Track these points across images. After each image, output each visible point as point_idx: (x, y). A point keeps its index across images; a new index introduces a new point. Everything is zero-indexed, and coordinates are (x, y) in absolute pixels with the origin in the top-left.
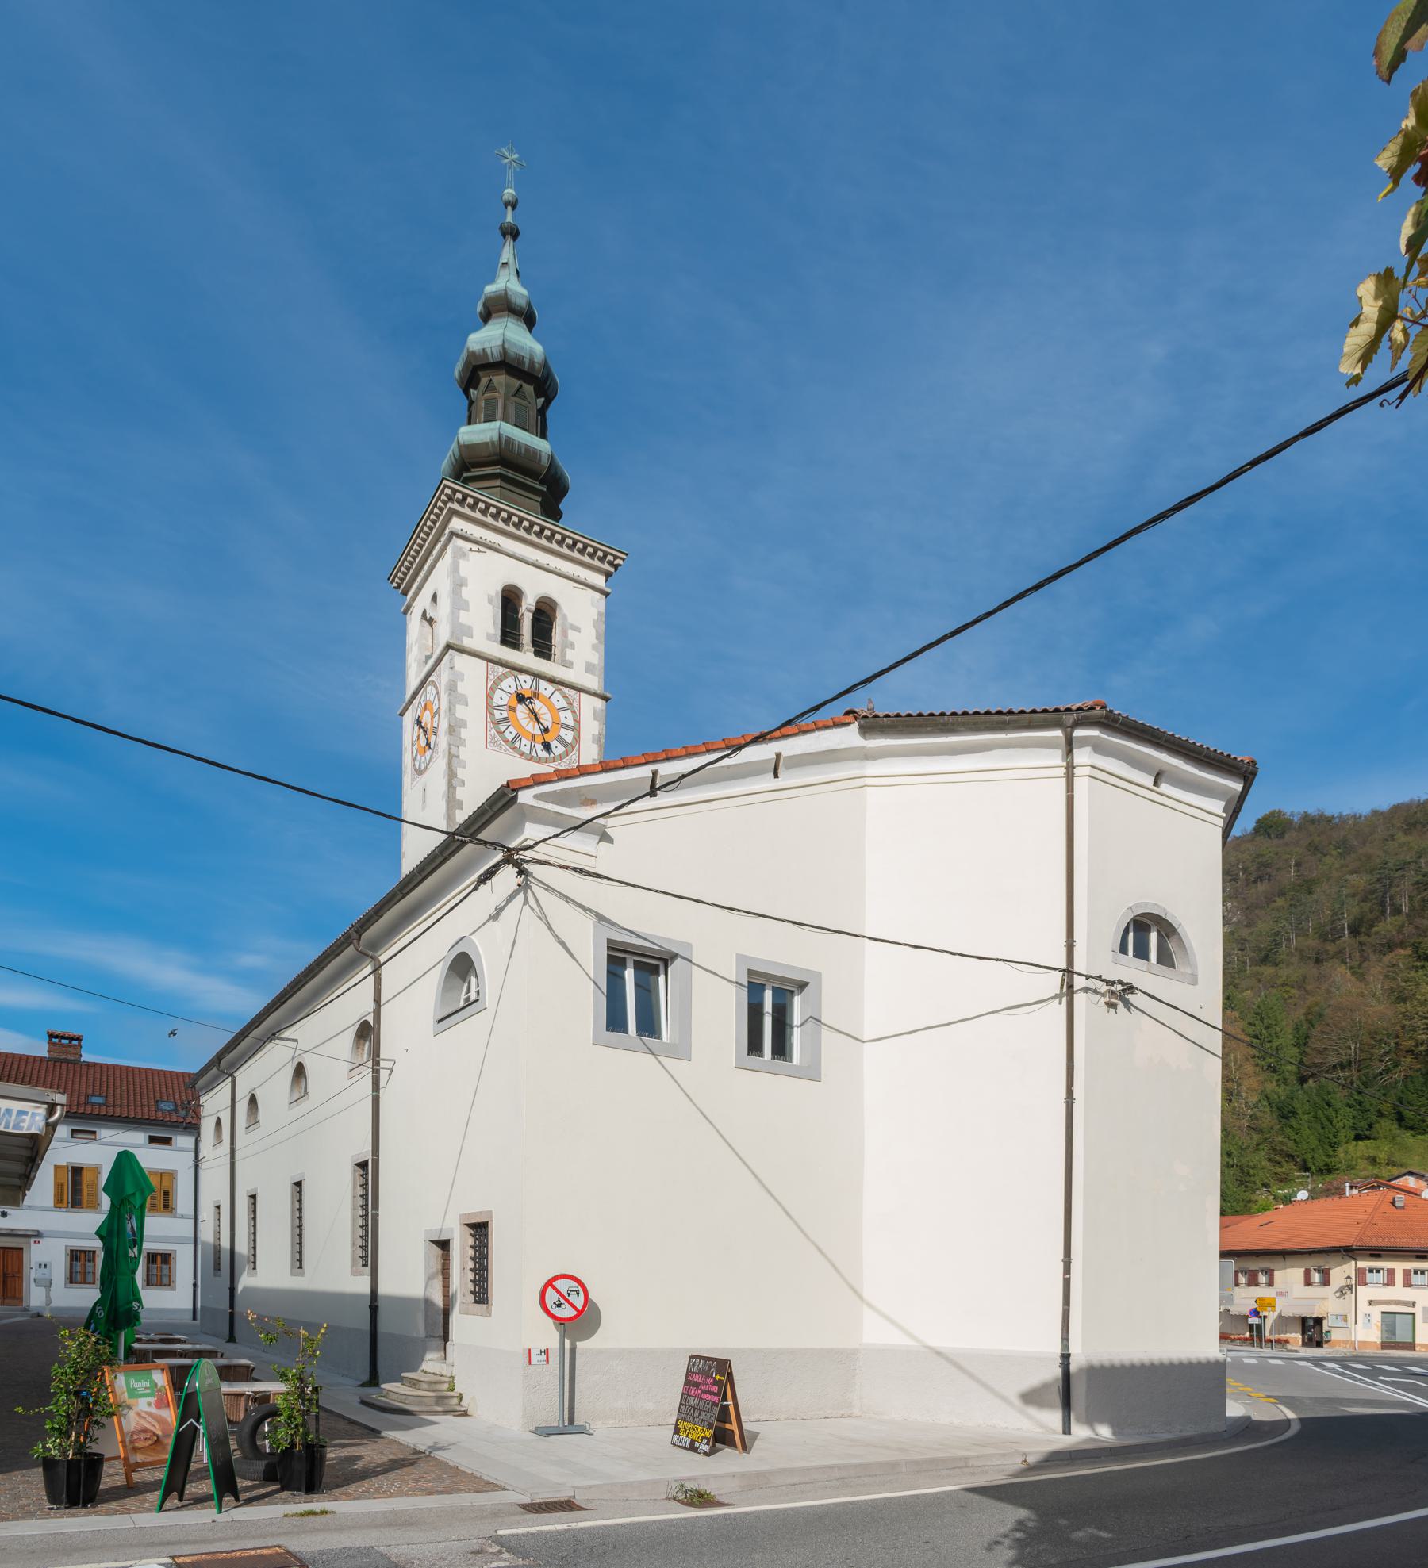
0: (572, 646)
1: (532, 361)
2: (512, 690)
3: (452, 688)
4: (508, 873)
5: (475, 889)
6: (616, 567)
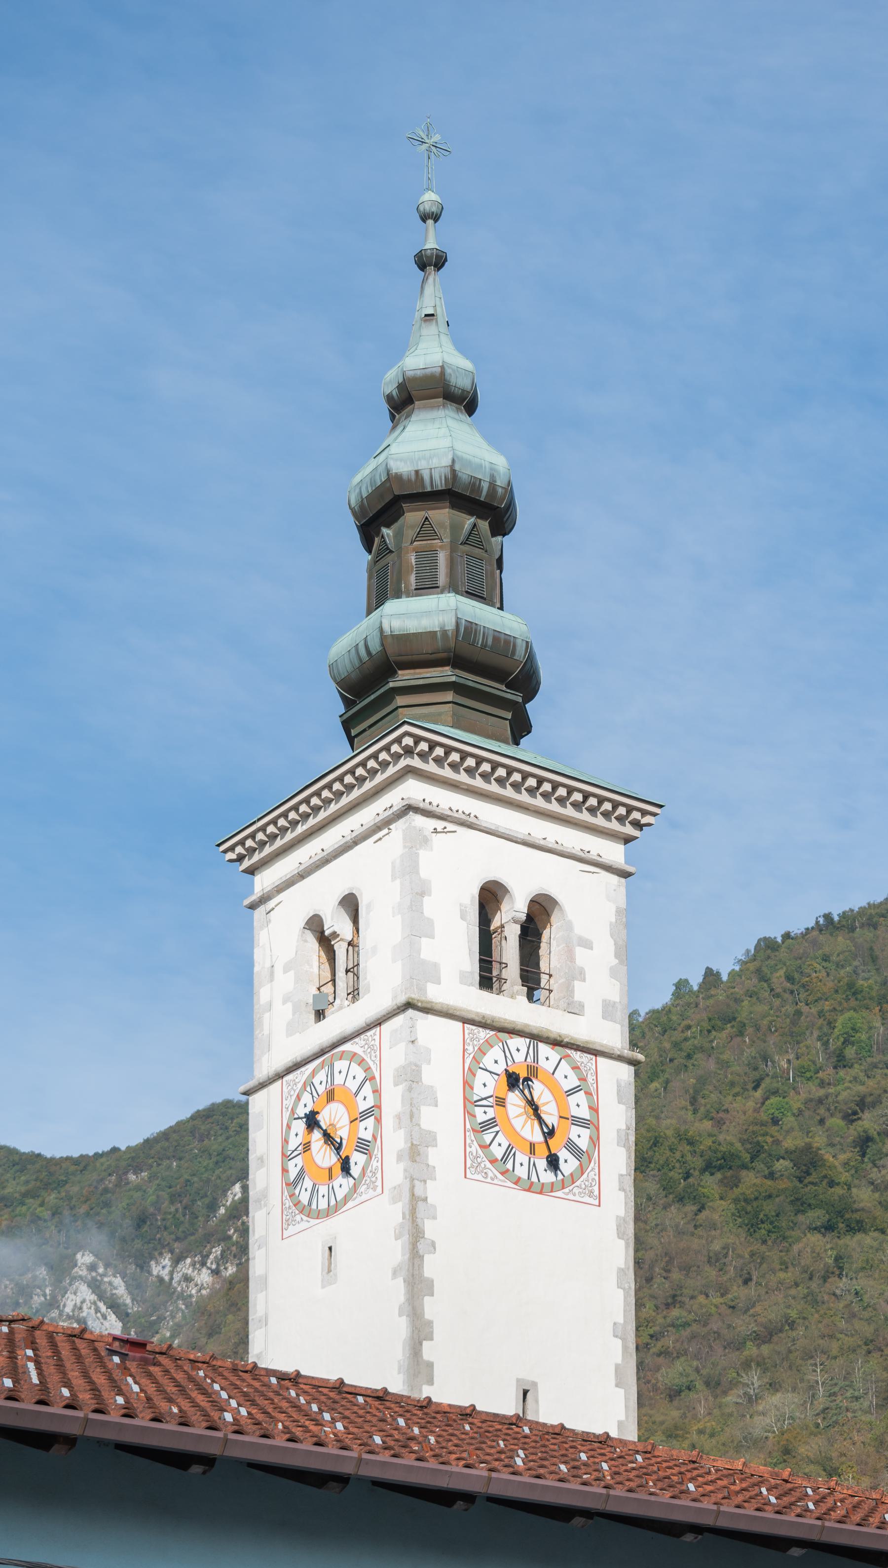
1: (492, 485)
2: (500, 1068)
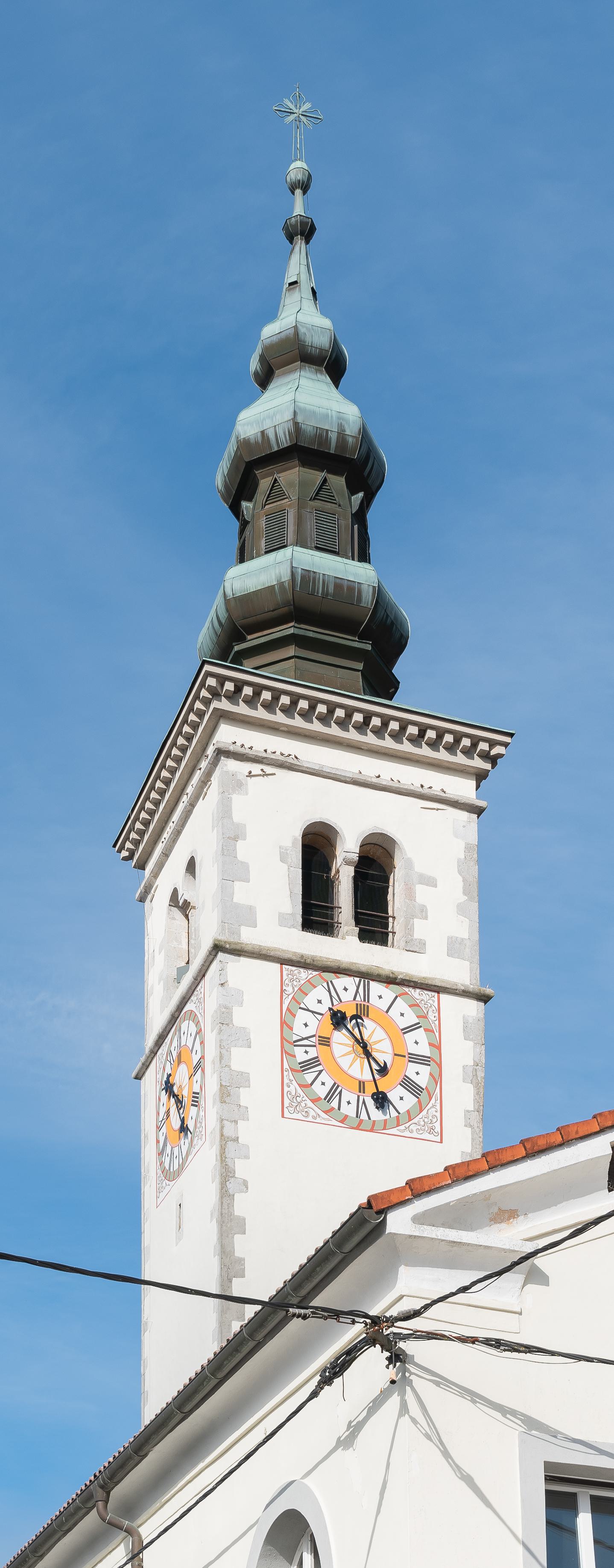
0: (423, 912)
1: (341, 435)
3: (224, 1020)
4: (373, 1363)
5: (314, 1394)
6: (494, 760)
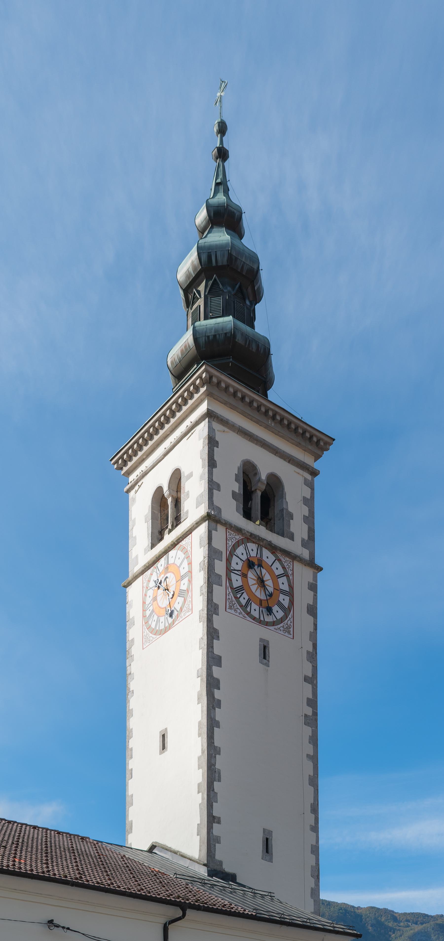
2: (244, 558)
